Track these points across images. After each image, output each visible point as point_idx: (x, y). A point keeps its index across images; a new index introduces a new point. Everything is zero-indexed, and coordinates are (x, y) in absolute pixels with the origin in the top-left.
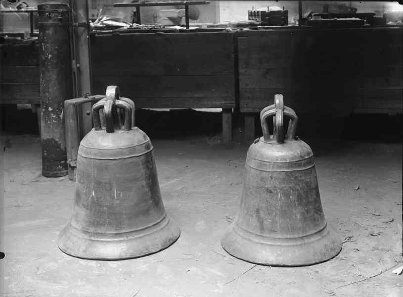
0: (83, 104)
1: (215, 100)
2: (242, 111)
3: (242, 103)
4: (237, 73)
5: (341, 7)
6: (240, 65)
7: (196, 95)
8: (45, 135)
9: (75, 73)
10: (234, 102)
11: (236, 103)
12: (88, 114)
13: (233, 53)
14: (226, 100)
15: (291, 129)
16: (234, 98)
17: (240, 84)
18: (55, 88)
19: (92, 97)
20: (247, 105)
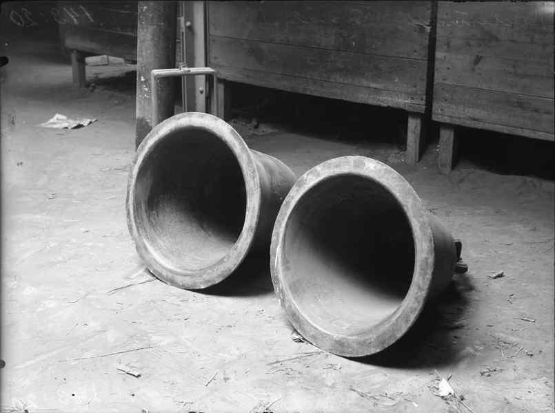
0: (197, 76)
1: (397, 95)
2: (435, 118)
3: (436, 107)
4: (431, 58)
5: (536, 134)
6: (438, 44)
7: (373, 85)
8: (138, 114)
9: (183, 33)
10: (424, 103)
11: (426, 105)
12: (202, 92)
13: (428, 26)
14: (412, 99)
15: (422, 251)
16: (424, 97)
17: (436, 75)
18: (149, 52)
19: (186, 69)
20: (442, 110)
